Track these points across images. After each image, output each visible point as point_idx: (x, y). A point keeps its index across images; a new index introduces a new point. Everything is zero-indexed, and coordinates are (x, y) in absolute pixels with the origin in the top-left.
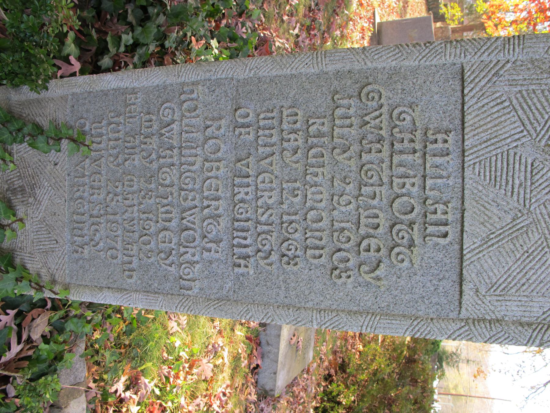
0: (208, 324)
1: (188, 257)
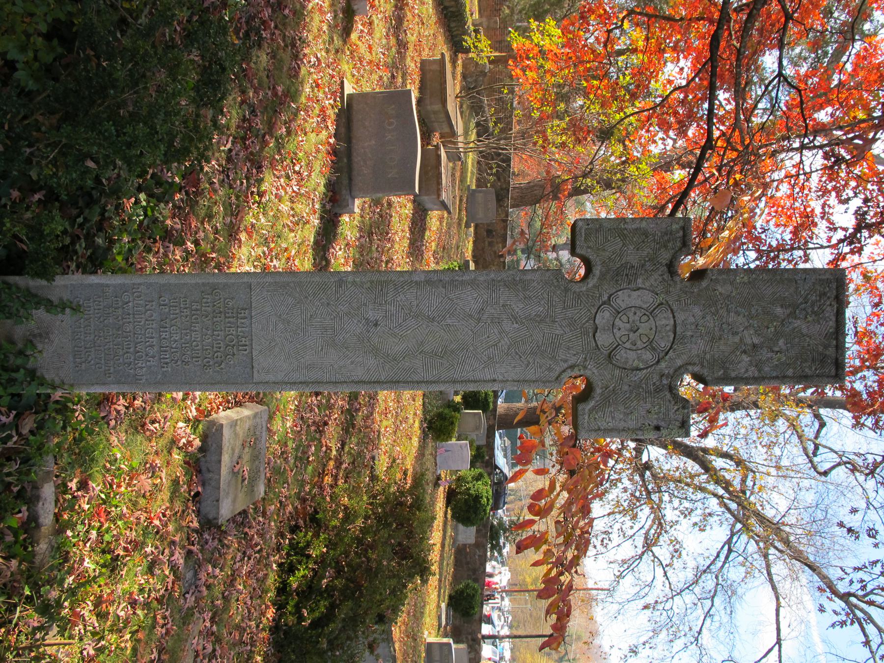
0: (145, 443)
1: (140, 365)
